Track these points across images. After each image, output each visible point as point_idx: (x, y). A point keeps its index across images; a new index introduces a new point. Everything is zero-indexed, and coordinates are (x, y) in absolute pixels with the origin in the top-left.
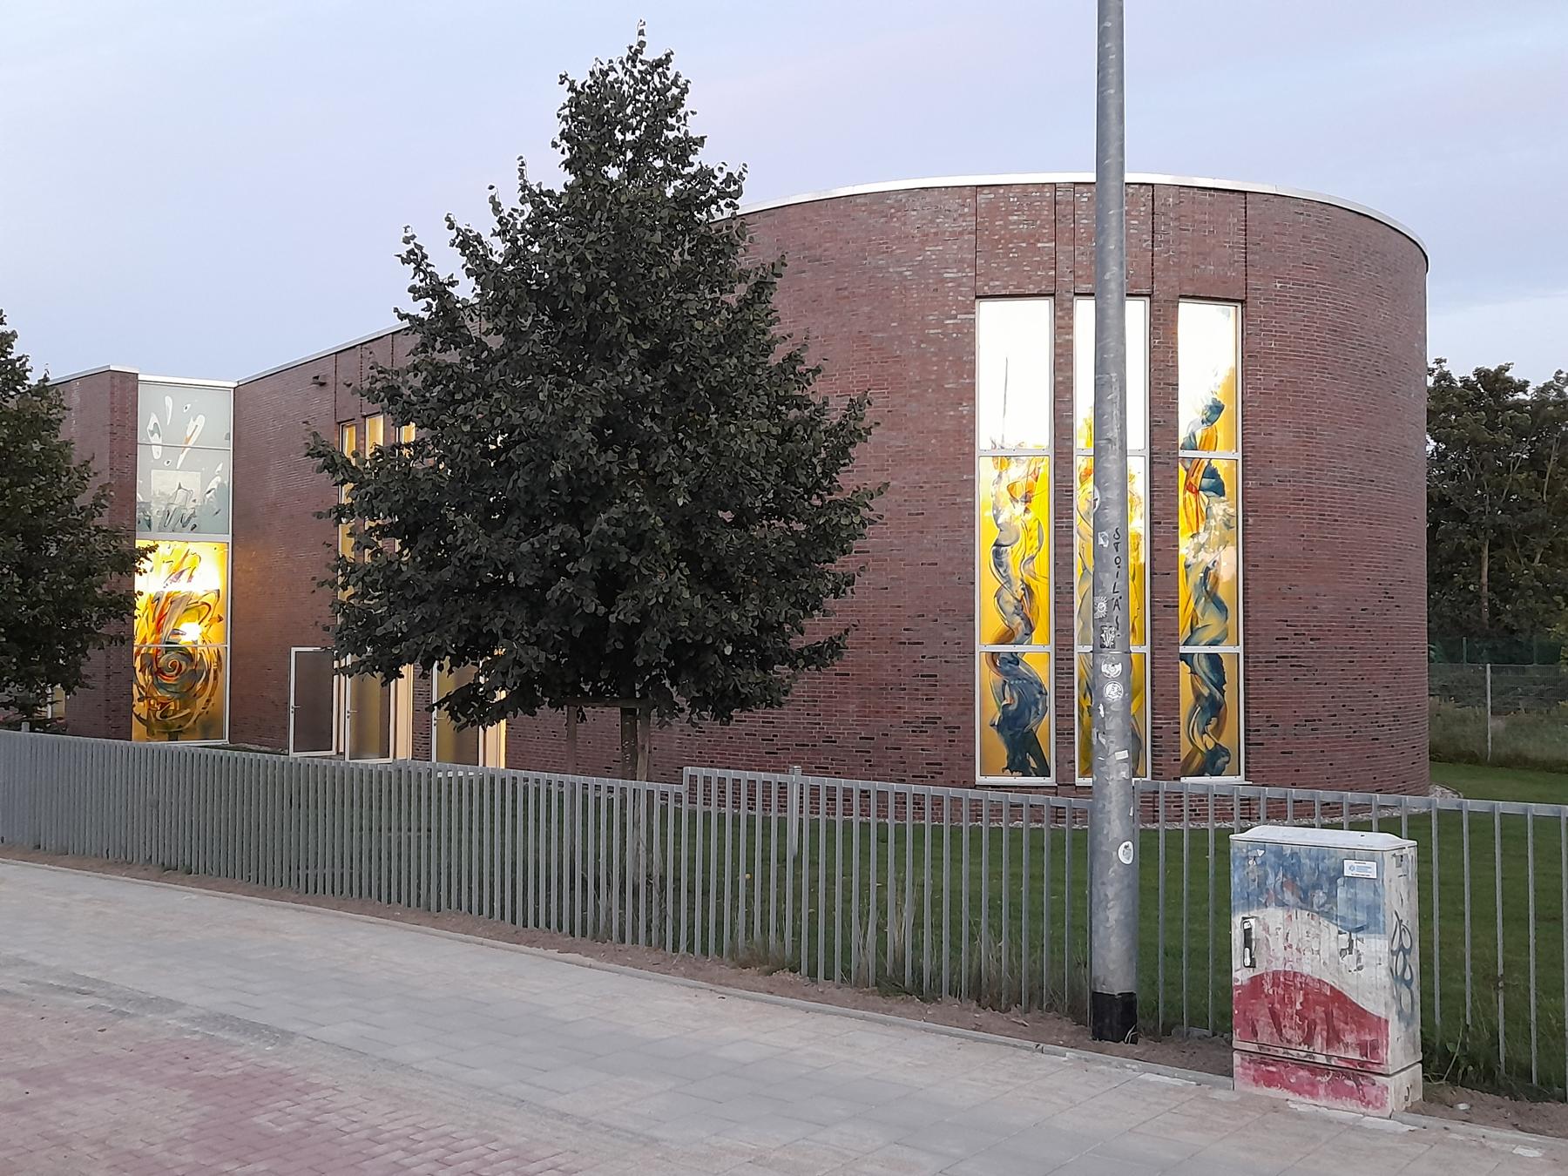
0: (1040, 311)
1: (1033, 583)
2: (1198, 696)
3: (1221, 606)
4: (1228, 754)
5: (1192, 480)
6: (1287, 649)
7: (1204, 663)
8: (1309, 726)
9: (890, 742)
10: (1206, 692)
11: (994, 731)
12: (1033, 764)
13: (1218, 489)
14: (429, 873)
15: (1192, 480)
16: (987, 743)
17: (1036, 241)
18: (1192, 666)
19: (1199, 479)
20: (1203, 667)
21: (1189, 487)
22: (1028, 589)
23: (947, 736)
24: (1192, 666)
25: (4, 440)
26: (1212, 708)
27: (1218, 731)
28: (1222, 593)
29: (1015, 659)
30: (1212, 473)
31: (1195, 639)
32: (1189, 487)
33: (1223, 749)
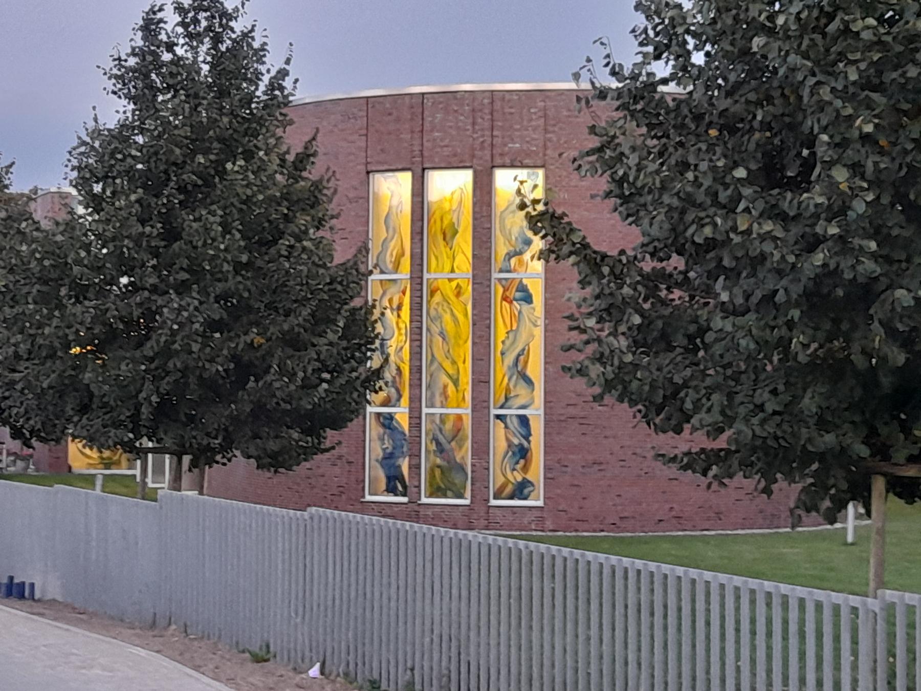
0: (405, 179)
1: (402, 365)
2: (510, 445)
3: (529, 382)
4: (533, 485)
5: (508, 293)
6: (572, 411)
7: (515, 420)
8: (596, 467)
9: (321, 471)
10: (516, 441)
11: (378, 466)
12: (400, 488)
13: (528, 299)
14: (693, 610)
15: (508, 293)
16: (375, 473)
17: (412, 131)
18: (506, 424)
19: (513, 293)
20: (514, 424)
21: (505, 298)
22: (399, 369)
23: (347, 467)
24: (506, 424)
25: (914, 62)
26: (522, 453)
27: (525, 469)
28: (529, 372)
29: (391, 417)
30: (522, 288)
31: (509, 403)
32: (505, 298)
33: (529, 482)
